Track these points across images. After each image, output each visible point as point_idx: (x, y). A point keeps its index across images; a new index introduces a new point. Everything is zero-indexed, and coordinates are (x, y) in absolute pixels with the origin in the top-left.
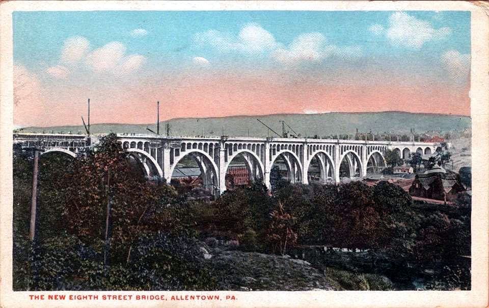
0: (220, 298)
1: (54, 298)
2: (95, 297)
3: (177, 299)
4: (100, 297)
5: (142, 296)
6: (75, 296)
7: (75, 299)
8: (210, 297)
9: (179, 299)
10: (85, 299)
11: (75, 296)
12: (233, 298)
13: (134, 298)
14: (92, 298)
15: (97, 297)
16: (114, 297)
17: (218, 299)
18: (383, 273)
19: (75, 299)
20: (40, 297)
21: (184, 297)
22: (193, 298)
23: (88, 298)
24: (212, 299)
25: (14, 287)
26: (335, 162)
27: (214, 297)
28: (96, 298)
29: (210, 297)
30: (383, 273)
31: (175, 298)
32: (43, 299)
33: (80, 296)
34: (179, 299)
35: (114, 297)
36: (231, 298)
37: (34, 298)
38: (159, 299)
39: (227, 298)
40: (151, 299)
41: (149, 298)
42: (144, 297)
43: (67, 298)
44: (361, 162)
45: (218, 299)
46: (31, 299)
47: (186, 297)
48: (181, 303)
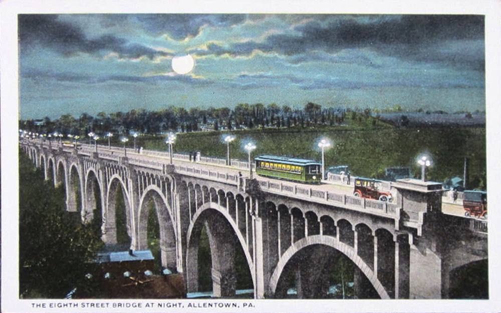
0: (237, 306)
1: (95, 305)
2: (37, 306)
3: (194, 306)
4: (47, 305)
5: (119, 304)
6: (55, 304)
7: (55, 306)
8: (228, 304)
9: (196, 307)
10: (175, 306)
11: (55, 304)
12: (251, 305)
13: (111, 305)
14: (72, 305)
15: (77, 305)
16: (92, 305)
17: (236, 306)
18: (452, 175)
19: (55, 306)
20: (41, 305)
21: (202, 305)
22: (211, 306)
23: (69, 305)
24: (229, 306)
25: (21, 292)
26: (99, 179)
27: (231, 305)
28: (76, 306)
29: (228, 304)
30: (452, 175)
31: (192, 305)
32: (141, 307)
33: (170, 303)
34: (196, 307)
35: (92, 305)
36: (248, 305)
37: (35, 306)
38: (170, 306)
39: (244, 306)
40: (127, 306)
41: (125, 305)
42: (120, 305)
43: (80, 306)
44: (126, 189)
45: (236, 306)
46: (33, 306)
47: (204, 305)
48: (198, 310)
